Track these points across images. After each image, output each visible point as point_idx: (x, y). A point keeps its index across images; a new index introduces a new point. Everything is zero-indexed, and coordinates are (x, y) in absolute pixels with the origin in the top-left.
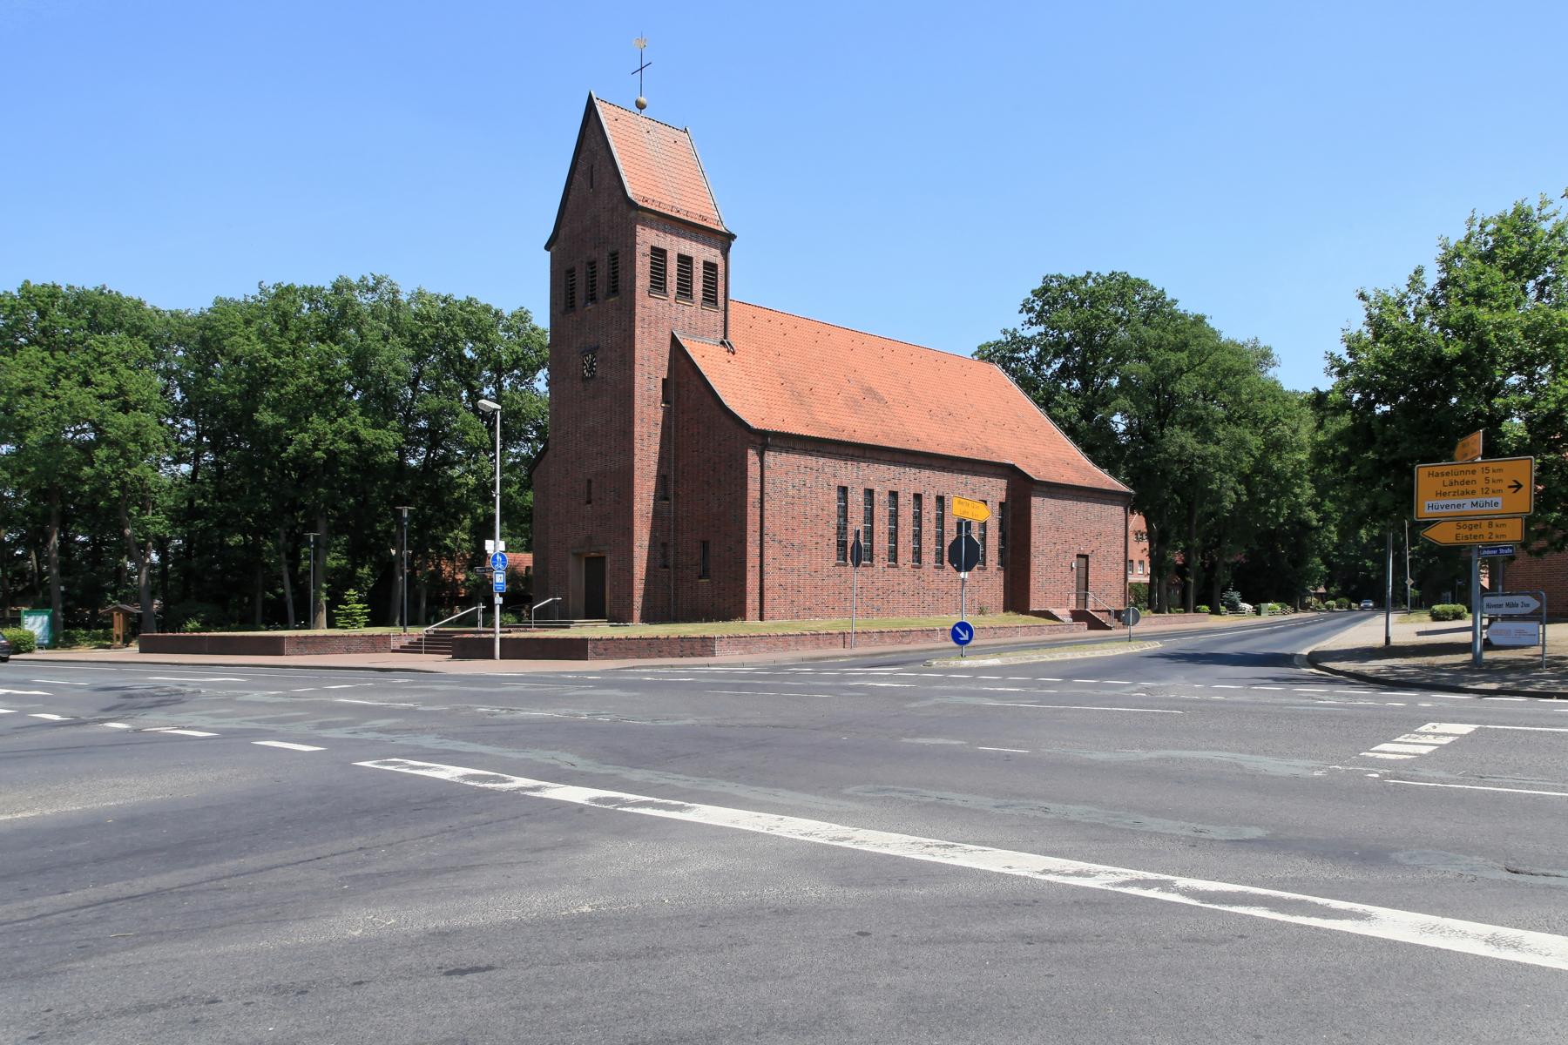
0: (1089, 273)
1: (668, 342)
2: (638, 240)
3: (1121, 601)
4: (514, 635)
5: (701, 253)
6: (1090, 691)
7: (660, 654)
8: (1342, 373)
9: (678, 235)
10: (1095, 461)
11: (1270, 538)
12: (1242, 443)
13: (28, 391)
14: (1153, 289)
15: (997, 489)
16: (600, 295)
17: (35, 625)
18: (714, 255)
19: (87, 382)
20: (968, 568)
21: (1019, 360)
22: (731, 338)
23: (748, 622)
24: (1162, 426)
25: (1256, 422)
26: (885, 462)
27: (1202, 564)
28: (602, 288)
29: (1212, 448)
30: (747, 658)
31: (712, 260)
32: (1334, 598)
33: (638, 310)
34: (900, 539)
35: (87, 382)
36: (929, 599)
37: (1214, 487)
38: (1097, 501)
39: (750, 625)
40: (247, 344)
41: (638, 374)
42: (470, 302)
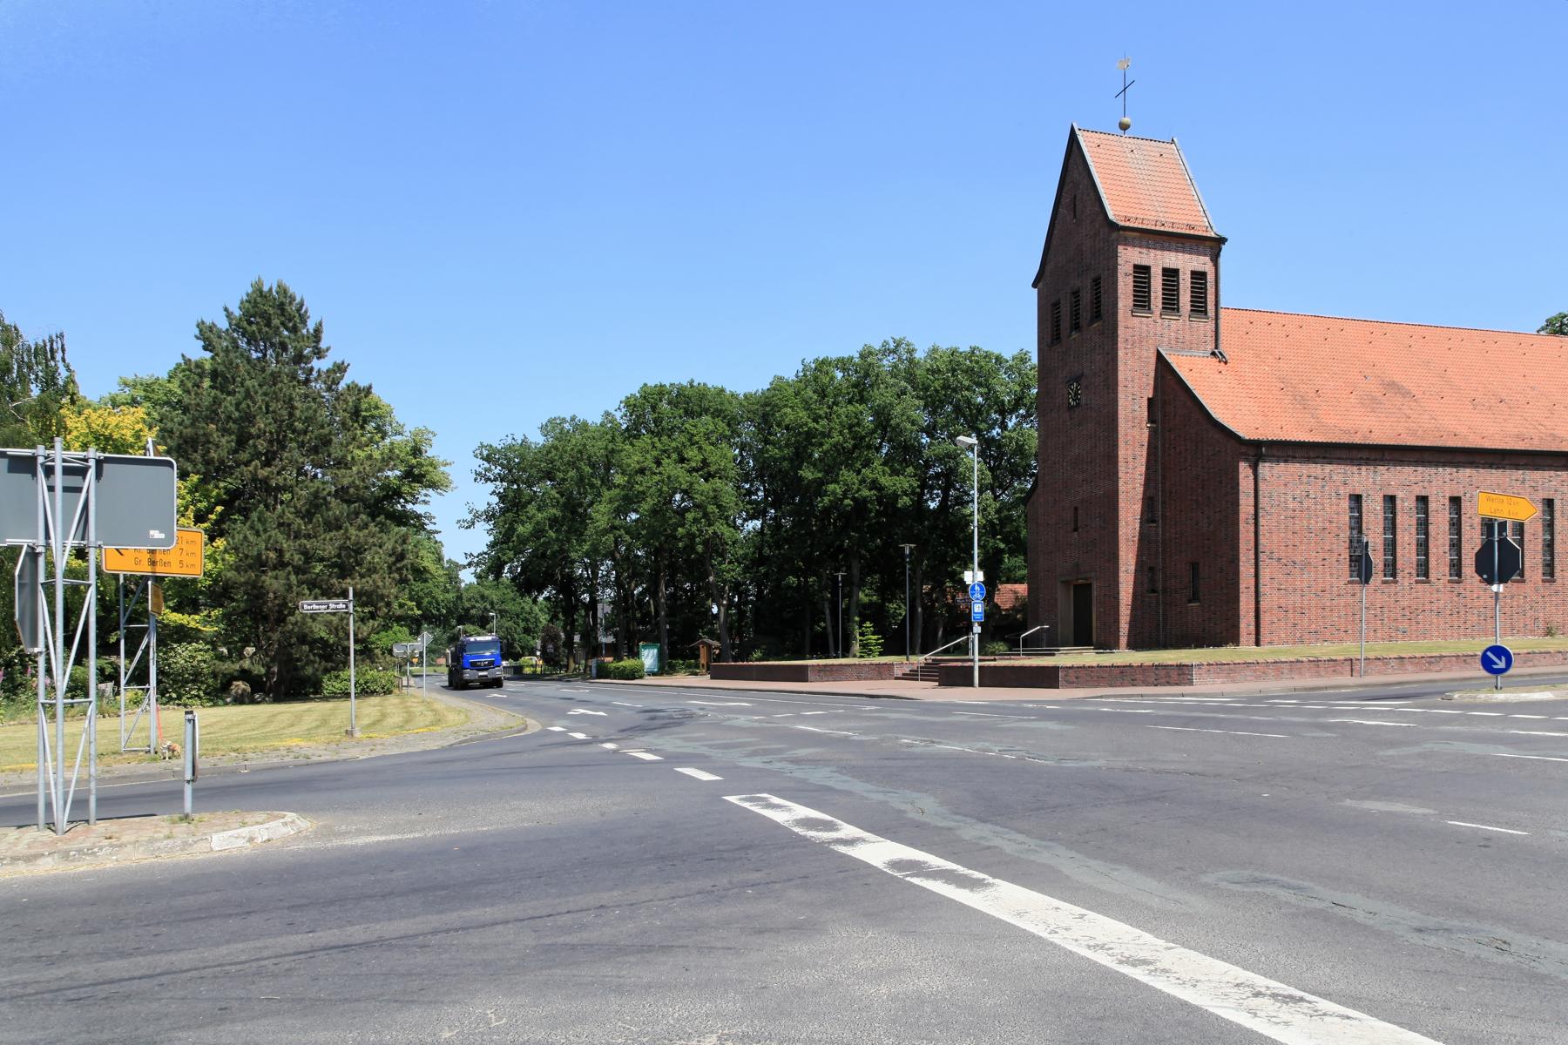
1: (1153, 360)
2: (1120, 261)
5: (1187, 263)
7: (1134, 683)
9: (1163, 249)
13: (642, 471)
16: (1083, 322)
17: (649, 657)
18: (1202, 263)
19: (682, 460)
22: (1222, 348)
23: (1241, 648)
28: (1085, 315)
30: (1230, 687)
31: (1200, 269)
34: (1432, 550)
35: (682, 460)
39: (1245, 651)
40: (794, 414)
41: (1121, 396)
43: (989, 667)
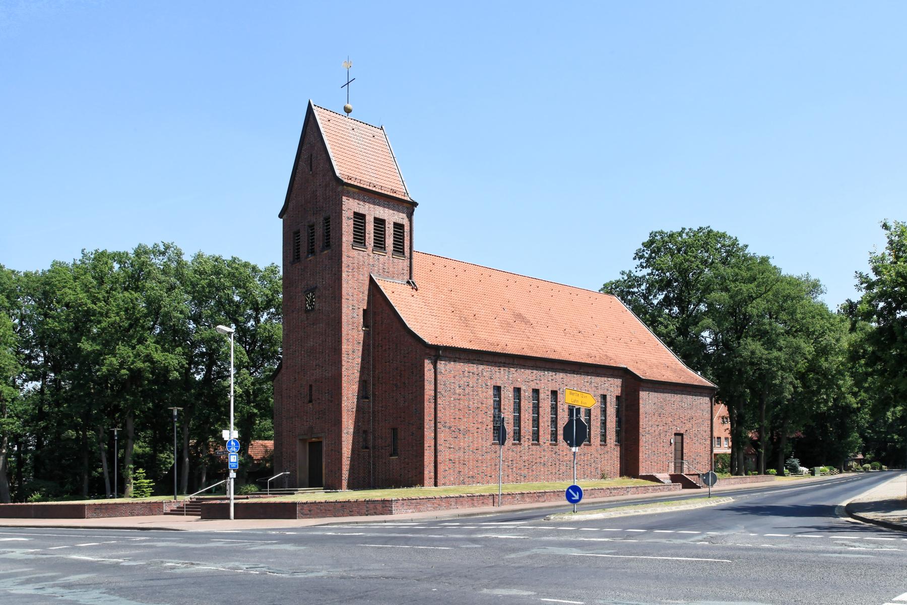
0: (684, 229)
1: (367, 282)
3: (708, 467)
4: (240, 501)
5: (391, 216)
6: (664, 541)
7: (324, 515)
8: (871, 286)
9: (374, 204)
10: (689, 364)
11: (822, 418)
12: (798, 349)
14: (730, 238)
15: (613, 387)
18: (401, 218)
20: (578, 445)
21: (634, 293)
22: (414, 279)
24: (739, 338)
25: (809, 334)
26: (528, 368)
27: (771, 439)
28: (319, 243)
29: (775, 353)
31: (400, 221)
32: (869, 462)
33: (344, 259)
34: (541, 424)
36: (563, 468)
37: (777, 382)
38: (689, 394)
39: (428, 490)
40: (74, 294)
41: (344, 305)
42: (234, 260)
43: (242, 504)
